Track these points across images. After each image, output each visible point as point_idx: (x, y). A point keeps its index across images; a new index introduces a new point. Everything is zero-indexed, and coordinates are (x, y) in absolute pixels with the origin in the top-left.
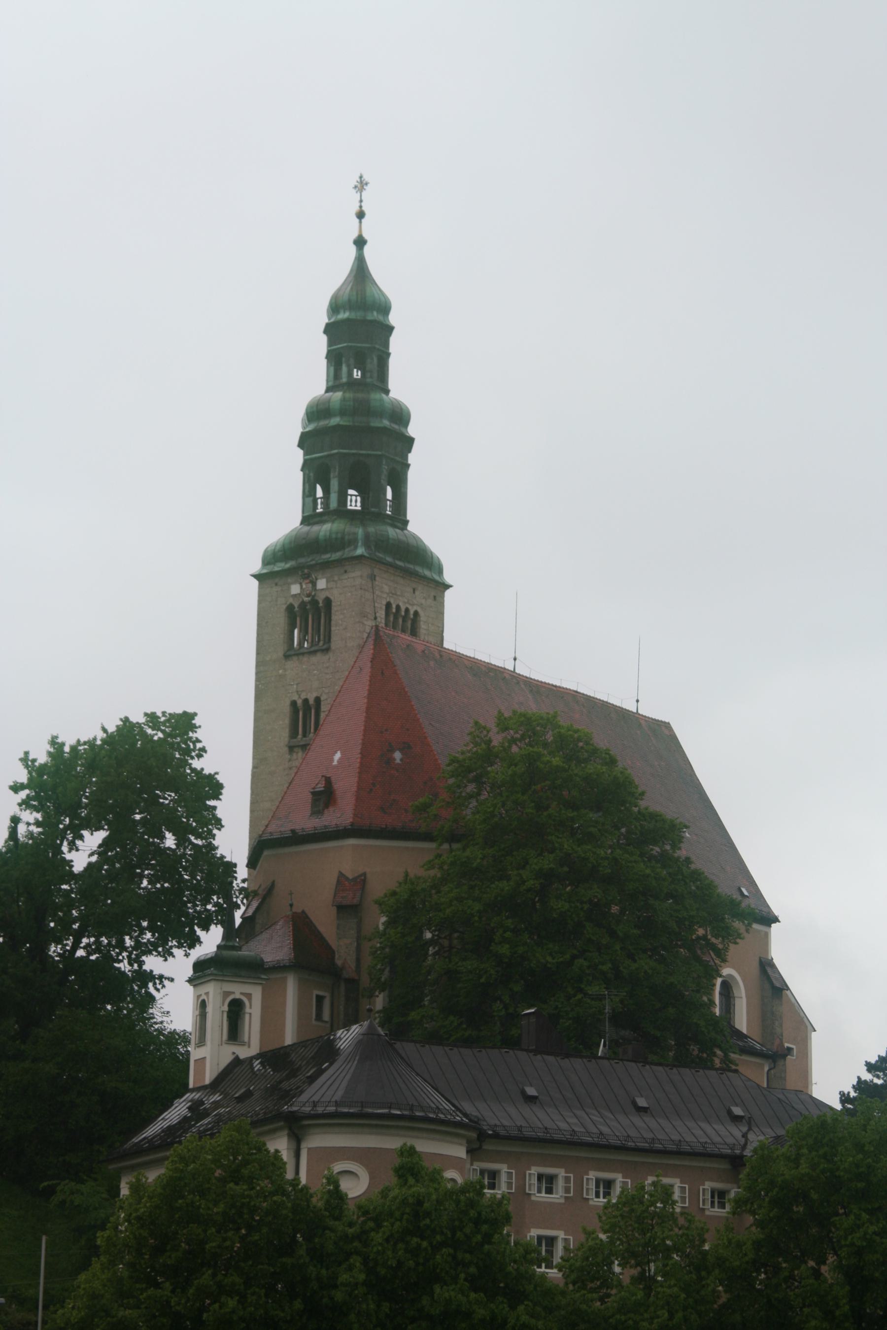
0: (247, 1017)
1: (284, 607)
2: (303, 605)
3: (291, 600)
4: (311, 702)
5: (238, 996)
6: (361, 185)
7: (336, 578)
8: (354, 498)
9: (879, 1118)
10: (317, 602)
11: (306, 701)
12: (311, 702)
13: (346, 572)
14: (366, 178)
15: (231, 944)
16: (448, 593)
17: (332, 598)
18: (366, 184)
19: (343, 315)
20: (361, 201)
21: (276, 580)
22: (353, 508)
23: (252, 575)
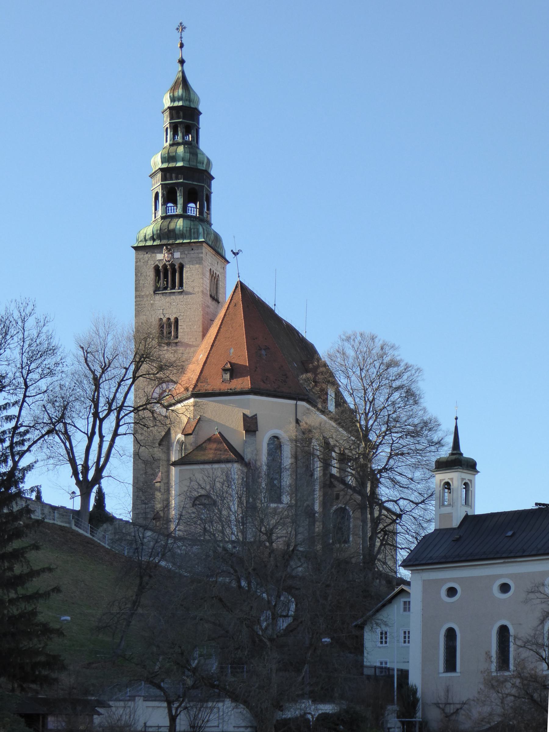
0: (470, 492)
1: (153, 266)
2: (165, 266)
3: (157, 263)
4: (172, 320)
5: (446, 480)
6: (182, 28)
7: (186, 252)
8: (172, 208)
9: (285, 598)
10: (174, 265)
11: (169, 319)
12: (172, 320)
13: (192, 249)
14: (185, 24)
15: (455, 452)
16: (228, 266)
17: (184, 264)
18: (185, 28)
19: (176, 104)
20: (181, 38)
21: (147, 251)
22: (192, 214)
23: (133, 247)
